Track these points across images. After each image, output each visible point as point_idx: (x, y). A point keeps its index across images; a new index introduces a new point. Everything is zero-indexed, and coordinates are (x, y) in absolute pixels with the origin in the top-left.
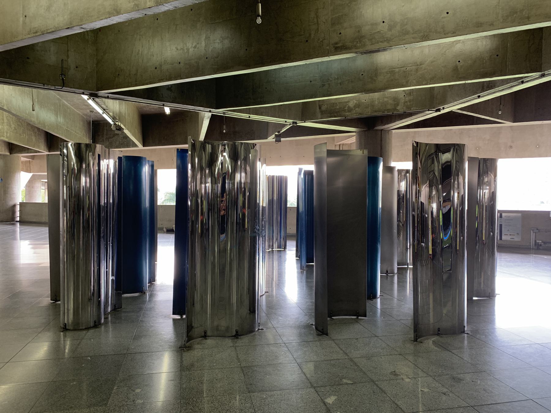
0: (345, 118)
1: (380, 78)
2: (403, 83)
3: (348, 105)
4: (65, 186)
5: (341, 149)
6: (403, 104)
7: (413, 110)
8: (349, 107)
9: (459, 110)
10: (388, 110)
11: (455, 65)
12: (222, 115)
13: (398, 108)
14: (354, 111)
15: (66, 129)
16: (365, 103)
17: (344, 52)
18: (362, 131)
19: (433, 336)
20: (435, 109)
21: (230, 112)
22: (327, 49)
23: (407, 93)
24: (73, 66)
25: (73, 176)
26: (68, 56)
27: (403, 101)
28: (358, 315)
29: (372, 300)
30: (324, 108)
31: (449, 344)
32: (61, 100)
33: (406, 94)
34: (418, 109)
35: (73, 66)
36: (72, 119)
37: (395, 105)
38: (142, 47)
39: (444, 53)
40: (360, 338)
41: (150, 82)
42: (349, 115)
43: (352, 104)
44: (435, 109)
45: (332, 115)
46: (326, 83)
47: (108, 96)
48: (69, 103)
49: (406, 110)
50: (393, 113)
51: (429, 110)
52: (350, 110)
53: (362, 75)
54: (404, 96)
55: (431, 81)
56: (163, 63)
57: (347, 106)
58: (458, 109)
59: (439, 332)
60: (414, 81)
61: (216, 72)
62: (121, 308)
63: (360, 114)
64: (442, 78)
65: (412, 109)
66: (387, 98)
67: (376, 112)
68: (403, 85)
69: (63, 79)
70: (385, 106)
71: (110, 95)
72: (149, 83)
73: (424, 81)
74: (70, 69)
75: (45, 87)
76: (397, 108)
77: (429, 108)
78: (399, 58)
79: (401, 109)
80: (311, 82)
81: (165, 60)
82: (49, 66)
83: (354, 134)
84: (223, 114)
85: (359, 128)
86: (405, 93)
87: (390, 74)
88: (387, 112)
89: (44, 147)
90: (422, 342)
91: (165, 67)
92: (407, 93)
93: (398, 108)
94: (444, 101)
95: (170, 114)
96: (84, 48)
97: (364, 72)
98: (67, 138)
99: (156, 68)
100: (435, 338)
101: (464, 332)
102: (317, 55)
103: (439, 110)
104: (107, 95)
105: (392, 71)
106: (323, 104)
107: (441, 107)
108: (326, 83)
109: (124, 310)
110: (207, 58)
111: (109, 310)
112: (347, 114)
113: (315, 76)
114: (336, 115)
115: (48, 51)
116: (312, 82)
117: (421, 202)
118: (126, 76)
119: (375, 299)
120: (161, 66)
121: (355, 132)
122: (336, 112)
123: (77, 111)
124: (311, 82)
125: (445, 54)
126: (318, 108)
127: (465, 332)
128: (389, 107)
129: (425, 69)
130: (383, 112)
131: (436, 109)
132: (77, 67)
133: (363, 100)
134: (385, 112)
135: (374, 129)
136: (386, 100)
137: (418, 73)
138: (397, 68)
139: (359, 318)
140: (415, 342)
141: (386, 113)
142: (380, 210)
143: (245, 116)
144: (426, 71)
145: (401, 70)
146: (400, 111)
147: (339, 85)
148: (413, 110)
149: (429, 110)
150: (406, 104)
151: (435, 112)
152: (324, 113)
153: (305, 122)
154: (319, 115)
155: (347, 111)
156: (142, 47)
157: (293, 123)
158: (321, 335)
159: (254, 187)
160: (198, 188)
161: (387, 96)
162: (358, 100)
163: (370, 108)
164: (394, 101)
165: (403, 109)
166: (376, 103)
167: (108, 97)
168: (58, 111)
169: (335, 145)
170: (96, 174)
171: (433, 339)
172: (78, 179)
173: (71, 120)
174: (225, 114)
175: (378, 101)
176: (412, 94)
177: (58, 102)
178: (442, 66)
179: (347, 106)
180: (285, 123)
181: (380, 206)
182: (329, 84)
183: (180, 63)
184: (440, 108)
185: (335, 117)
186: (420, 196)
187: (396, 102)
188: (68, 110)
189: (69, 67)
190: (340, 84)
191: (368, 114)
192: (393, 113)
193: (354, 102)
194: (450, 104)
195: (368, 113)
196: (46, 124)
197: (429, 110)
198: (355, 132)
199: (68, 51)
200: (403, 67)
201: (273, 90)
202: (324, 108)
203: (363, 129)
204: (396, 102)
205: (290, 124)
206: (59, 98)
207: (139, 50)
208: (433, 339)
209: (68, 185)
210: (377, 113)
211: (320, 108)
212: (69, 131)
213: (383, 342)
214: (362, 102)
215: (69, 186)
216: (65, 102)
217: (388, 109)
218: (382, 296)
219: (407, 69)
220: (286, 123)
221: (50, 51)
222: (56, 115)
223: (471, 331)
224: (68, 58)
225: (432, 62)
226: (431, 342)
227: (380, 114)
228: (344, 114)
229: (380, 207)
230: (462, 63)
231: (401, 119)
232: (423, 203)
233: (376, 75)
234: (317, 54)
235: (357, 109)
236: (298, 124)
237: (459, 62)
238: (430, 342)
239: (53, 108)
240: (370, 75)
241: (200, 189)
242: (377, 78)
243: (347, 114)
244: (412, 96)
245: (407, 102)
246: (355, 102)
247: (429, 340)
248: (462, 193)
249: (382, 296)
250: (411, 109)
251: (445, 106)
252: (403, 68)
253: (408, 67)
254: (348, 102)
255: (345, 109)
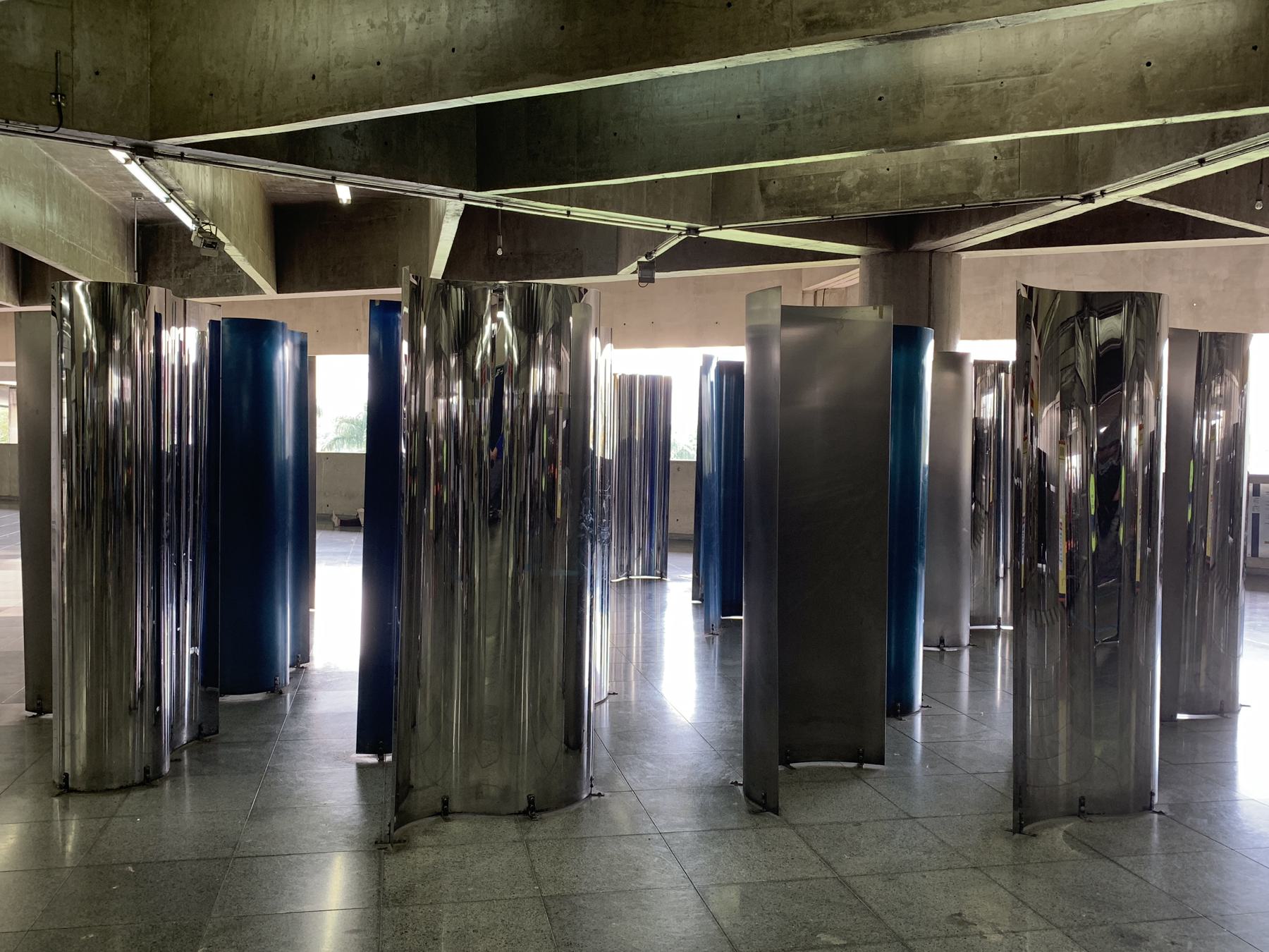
0: (833, 218)
1: (930, 108)
2: (993, 122)
3: (840, 181)
4: (65, 400)
5: (819, 304)
6: (990, 181)
7: (1018, 198)
8: (842, 188)
9: (1145, 199)
10: (951, 198)
11: (1137, 72)
12: (495, 207)
13: (979, 191)
14: (858, 199)
15: (66, 243)
16: (887, 176)
17: (831, 35)
18: (878, 255)
19: (1066, 819)
20: (1078, 196)
21: (515, 200)
22: (786, 28)
23: (1002, 151)
24: (86, 69)
25: (87, 371)
26: (73, 43)
27: (991, 173)
28: (860, 758)
29: (901, 720)
30: (773, 189)
31: (1110, 842)
32: (52, 163)
33: (1001, 154)
34: (1031, 194)
35: (86, 69)
36: (83, 216)
37: (968, 182)
38: (277, 18)
39: (1108, 41)
40: (865, 821)
41: (297, 115)
42: (844, 209)
43: (850, 181)
44: (1078, 196)
45: (797, 208)
46: (777, 122)
47: (182, 154)
48: (74, 172)
49: (1000, 196)
50: (963, 206)
51: (1062, 199)
52: (845, 196)
53: (880, 99)
54: (996, 158)
55: (1069, 118)
56: (333, 63)
57: (838, 184)
58: (1144, 196)
59: (1082, 808)
60: (1024, 118)
61: (480, 88)
62: (217, 732)
63: (874, 207)
64: (1101, 111)
65: (1017, 194)
66: (949, 164)
67: (916, 201)
68: (991, 128)
69: (59, 105)
70: (943, 185)
71: (187, 151)
72: (294, 119)
73: (1051, 117)
74: (79, 80)
75: (9, 128)
76: (975, 192)
77: (1061, 193)
78: (981, 54)
79: (985, 193)
80: (739, 117)
81: (338, 55)
82: (22, 67)
83: (856, 261)
84: (497, 205)
85: (872, 245)
86: (999, 151)
87: (956, 98)
88: (945, 202)
89: (7, 291)
90: (1035, 835)
91: (338, 75)
92: (1002, 151)
93: (979, 191)
94: (1105, 175)
95: (350, 202)
96: (117, 21)
97: (886, 91)
98: (69, 268)
99: (314, 77)
100: (1070, 825)
101: (1150, 808)
102: (756, 45)
103: (1089, 198)
104: (178, 151)
105: (963, 90)
106: (770, 180)
107: (1097, 191)
108: (777, 122)
109: (225, 739)
110: (453, 50)
111: (185, 737)
112: (837, 206)
113: (750, 100)
114: (805, 209)
115: (19, 29)
116: (742, 119)
117: (1039, 451)
118: (233, 100)
119: (909, 717)
120: (328, 71)
121: (859, 257)
122: (808, 201)
123: (98, 194)
124: (739, 117)
125: (1110, 44)
126: (757, 189)
127: (1155, 809)
128: (953, 188)
129: (1053, 86)
130: (938, 203)
131: (1083, 196)
132: (97, 73)
133: (882, 168)
134: (943, 203)
135: (912, 249)
136: (944, 168)
137: (1034, 96)
138: (977, 81)
139: (865, 766)
140: (1017, 835)
141: (944, 205)
142: (924, 473)
143: (555, 210)
144: (1056, 89)
145: (986, 86)
146: (984, 200)
147: (817, 126)
148: (1020, 196)
149: (1062, 197)
150: (1000, 180)
151: (1078, 202)
152: (773, 202)
153: (721, 228)
154: (760, 209)
155: (837, 198)
156: (277, 18)
157: (689, 230)
158: (761, 811)
159: (581, 407)
160: (427, 409)
161: (947, 158)
162: (867, 170)
163: (900, 188)
164: (967, 172)
165: (991, 193)
166: (918, 176)
167: (181, 157)
168: (44, 193)
169: (804, 293)
170: (149, 365)
171: (1065, 827)
172: (101, 380)
173: (80, 218)
174: (502, 205)
175: (923, 171)
176: (1016, 153)
177: (45, 167)
178: (1101, 77)
179: (838, 184)
180: (666, 231)
181: (925, 459)
182: (788, 124)
183: (378, 63)
184: (1093, 194)
185: (804, 214)
186: (1037, 435)
187: (972, 176)
188: (74, 190)
189: (75, 73)
190: (820, 123)
191: (896, 207)
192: (963, 206)
193: (855, 174)
194: (1122, 182)
195: (895, 204)
196: (13, 229)
197: (1062, 197)
198: (859, 257)
199: (72, 28)
200: (993, 79)
201: (635, 138)
202: (773, 189)
203: (880, 250)
204: (972, 176)
205: (680, 235)
206: (48, 159)
207: (268, 27)
208: (1065, 827)
209: (73, 398)
210: (918, 206)
211: (763, 190)
212: (75, 247)
213: (928, 833)
214: (879, 176)
215: (76, 400)
216: (66, 169)
217: (949, 195)
218: (928, 707)
219: (1005, 84)
220: (670, 231)
221: (23, 27)
222: (41, 205)
223: (1170, 805)
224: (73, 49)
225: (1073, 66)
226: (1061, 834)
227: (928, 207)
228: (826, 207)
229: (924, 464)
230: (1154, 70)
231: (985, 224)
232: (1045, 454)
233: (918, 101)
234: (756, 42)
235: (864, 194)
236: (701, 235)
237: (1149, 64)
238: (1059, 835)
239: (31, 184)
240: (902, 100)
241: (433, 410)
242: (919, 106)
243: (837, 206)
244: (1018, 159)
245: (1001, 175)
246: (860, 173)
247: (1055, 829)
248: (1152, 427)
249: (928, 707)
250: (1012, 196)
251: (1108, 188)
252: (993, 82)
253: (1007, 77)
254: (841, 173)
255: (832, 192)
